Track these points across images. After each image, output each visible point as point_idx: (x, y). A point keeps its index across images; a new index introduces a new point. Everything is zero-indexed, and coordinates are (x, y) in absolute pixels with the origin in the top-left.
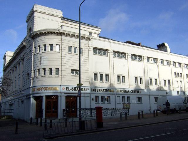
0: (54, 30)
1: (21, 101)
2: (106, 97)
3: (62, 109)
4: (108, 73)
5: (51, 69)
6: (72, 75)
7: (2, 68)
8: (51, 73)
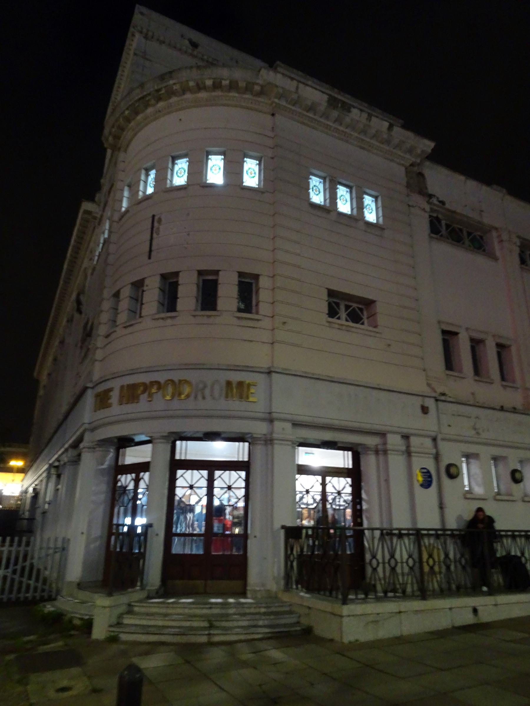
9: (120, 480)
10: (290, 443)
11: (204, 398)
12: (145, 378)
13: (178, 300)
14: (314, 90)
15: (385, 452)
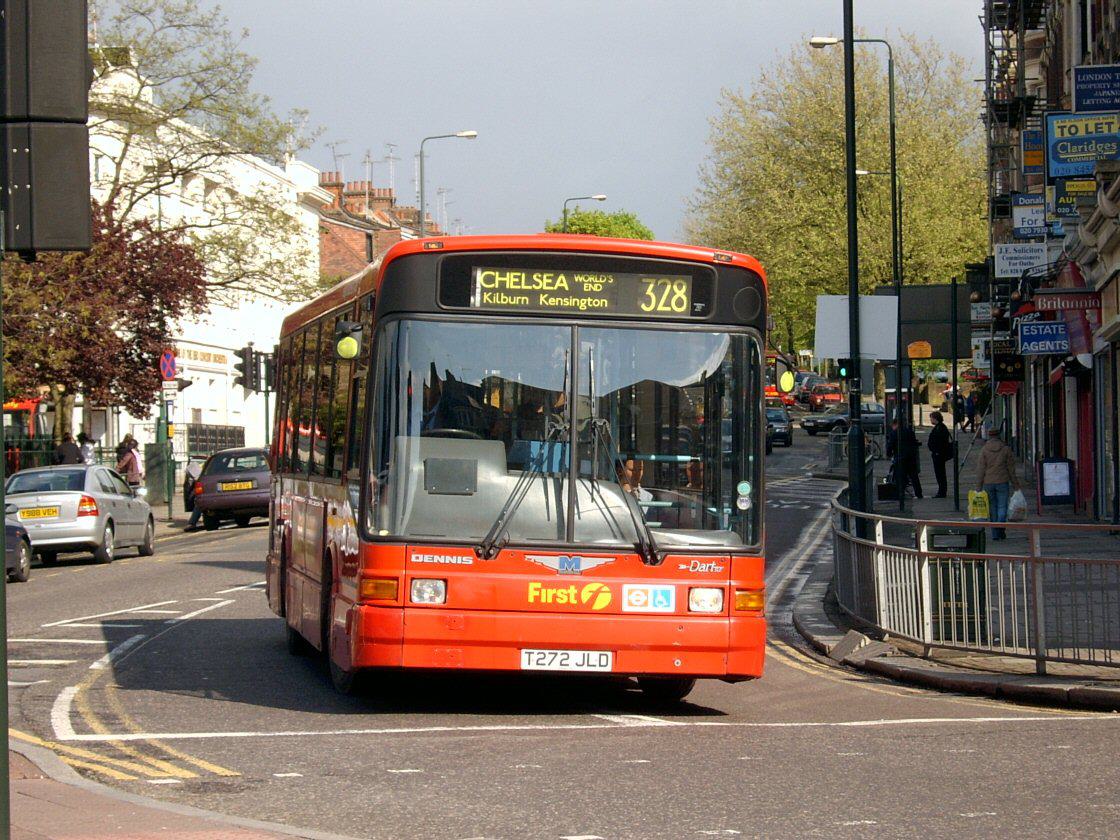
9: (994, 316)
11: (699, 190)
13: (983, 6)
14: (31, 103)
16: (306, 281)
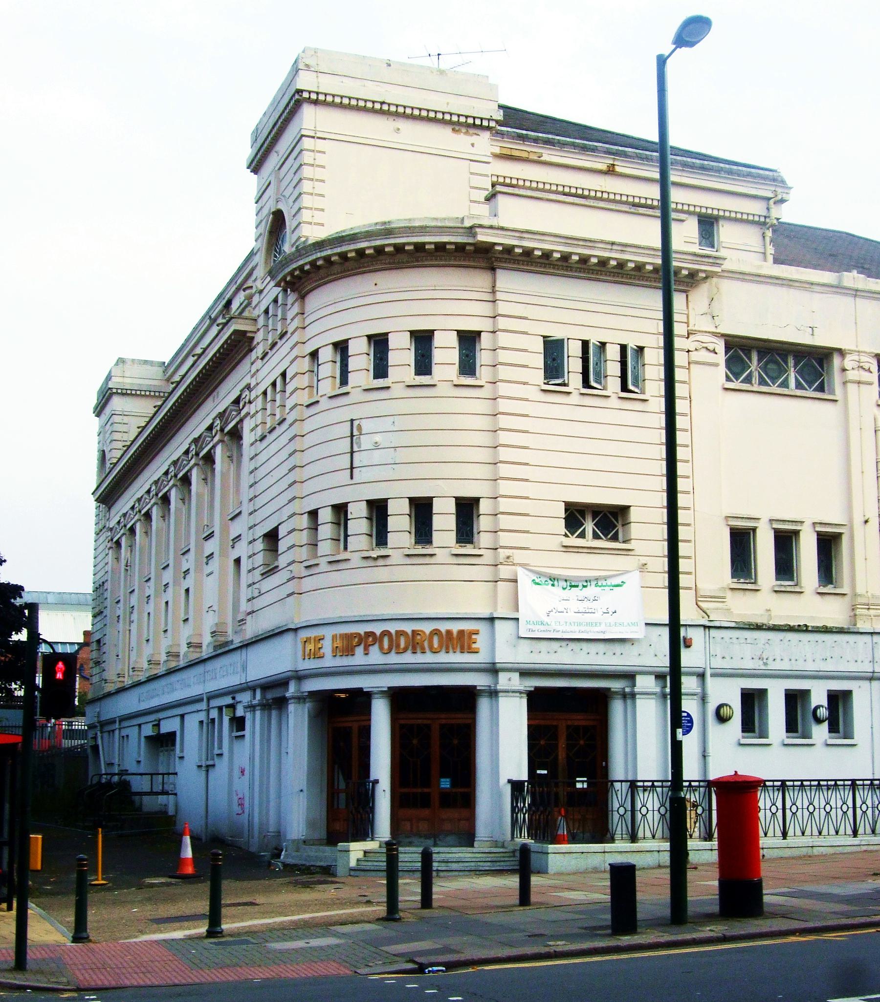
0: (441, 230)
1: (226, 719)
2: (819, 698)
3: (503, 781)
4: (832, 515)
5: (422, 509)
6: (573, 541)
7: (87, 478)
8: (424, 365)
10: (518, 694)
12: (361, 629)
15: (633, 696)
16: (728, 379)
